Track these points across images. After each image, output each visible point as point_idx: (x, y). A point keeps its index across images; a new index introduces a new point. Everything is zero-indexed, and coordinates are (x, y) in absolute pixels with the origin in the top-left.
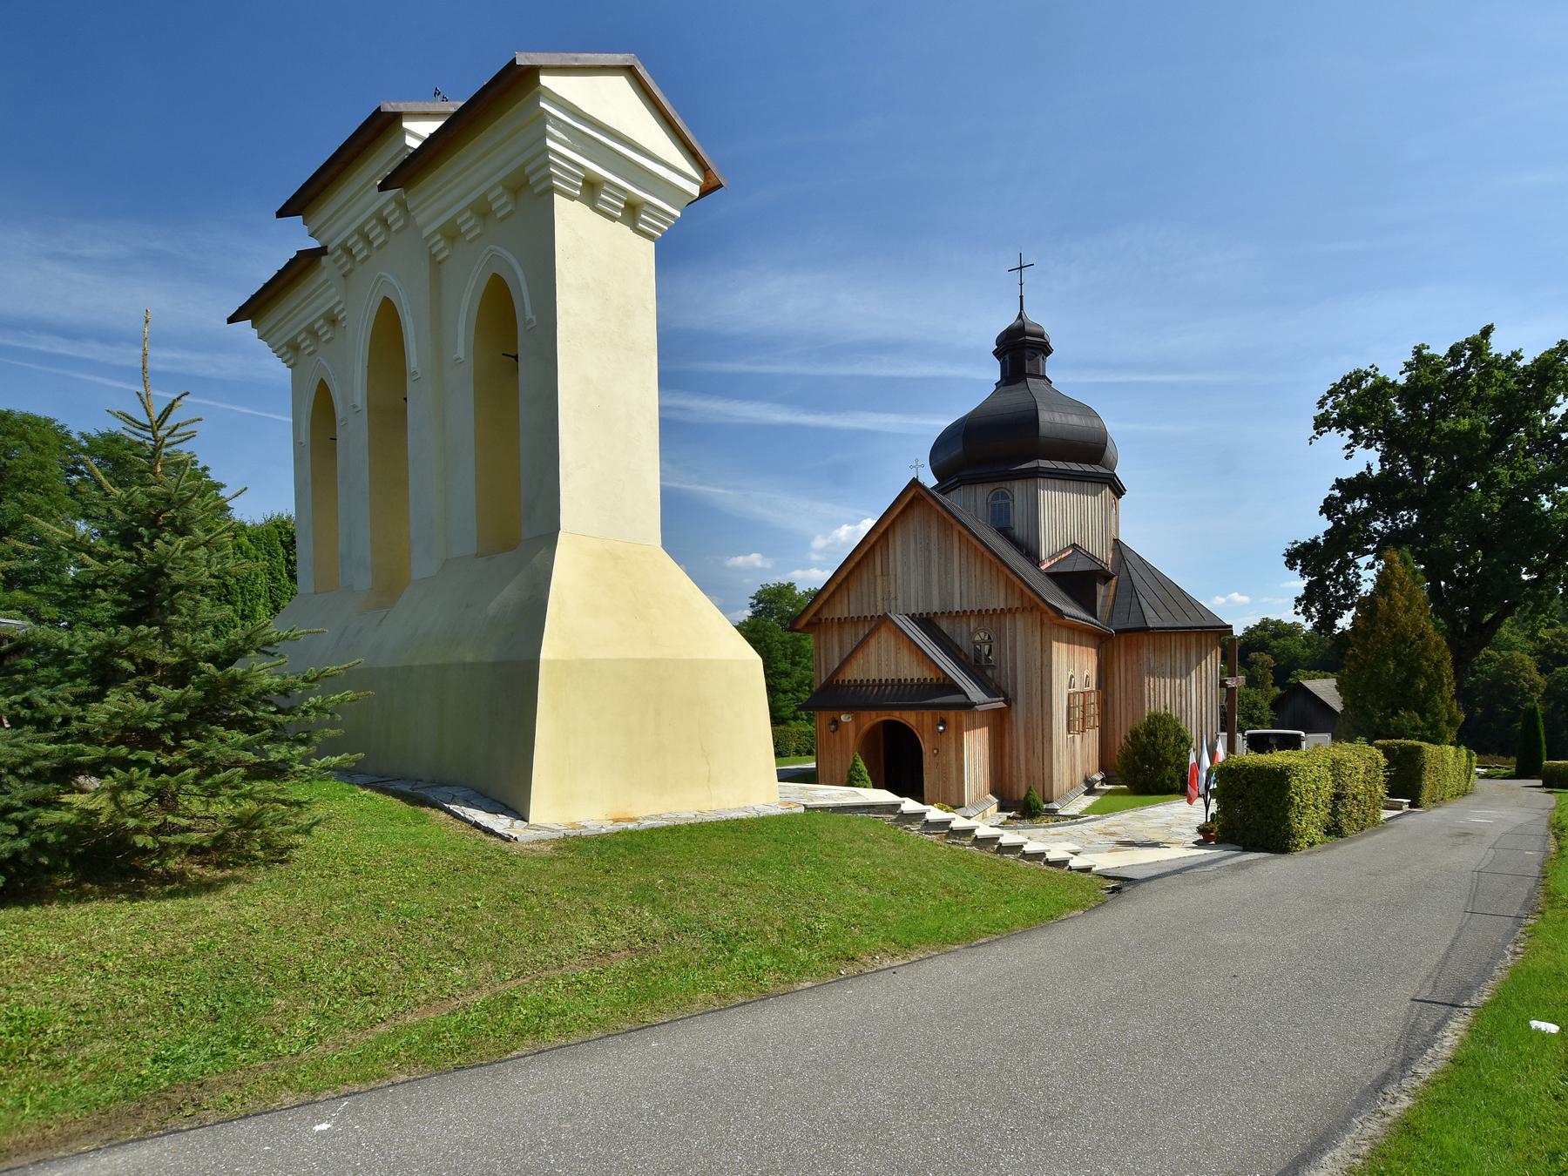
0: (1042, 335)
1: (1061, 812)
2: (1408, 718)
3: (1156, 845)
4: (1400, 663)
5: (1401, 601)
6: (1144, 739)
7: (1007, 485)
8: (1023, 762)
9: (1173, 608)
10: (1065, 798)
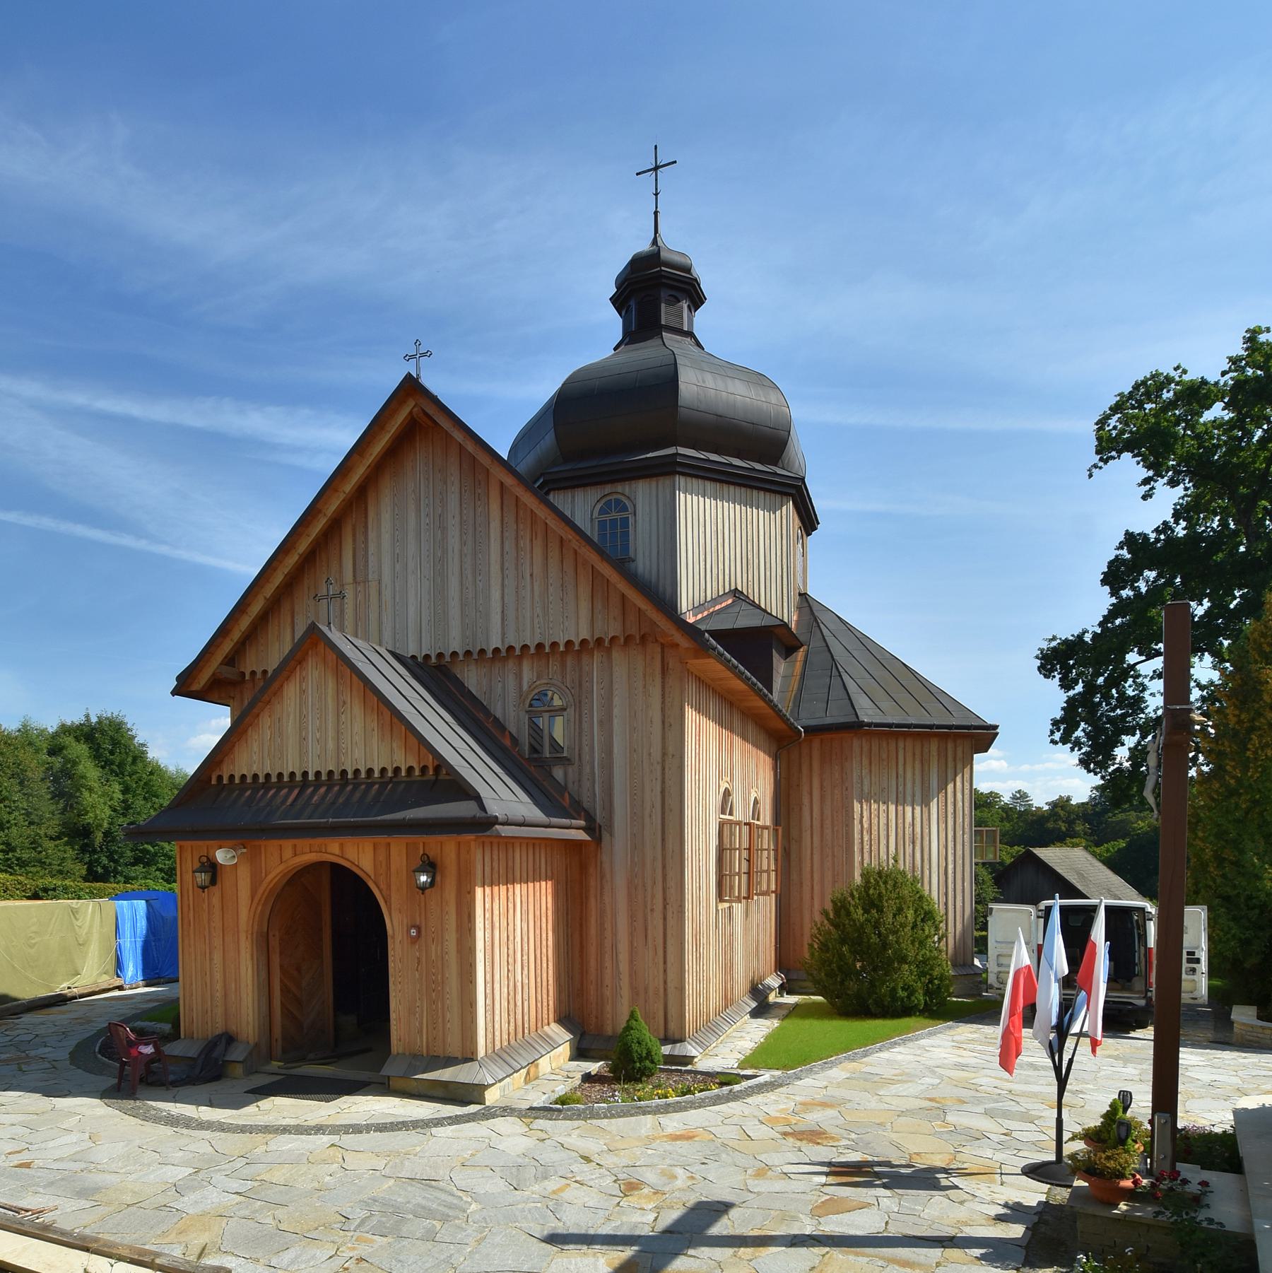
1: (704, 1063)
3: (926, 1179)
6: (859, 914)
8: (623, 957)
9: (903, 697)
10: (711, 1028)
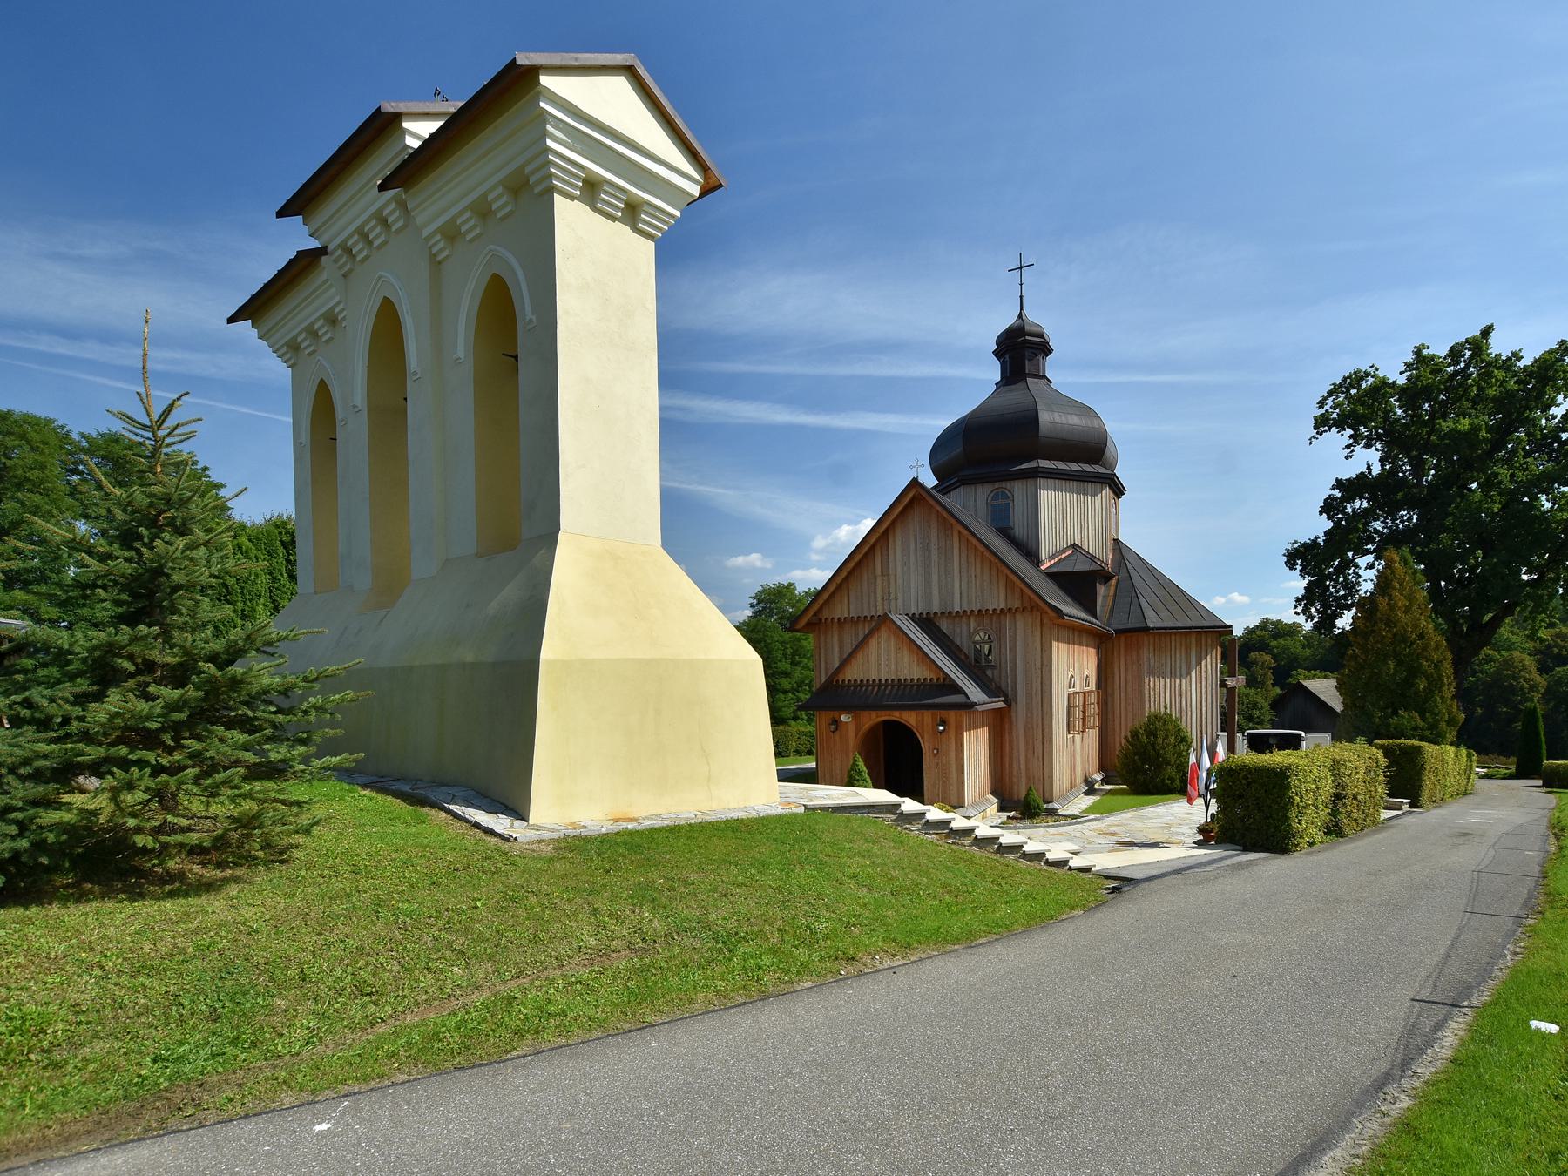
0: (1042, 335)
1: (1061, 812)
2: (1408, 718)
3: (1156, 845)
4: (1400, 663)
5: (1401, 601)
6: (1144, 739)
7: (1007, 485)
8: (1023, 762)
9: (1173, 608)
10: (1065, 798)
